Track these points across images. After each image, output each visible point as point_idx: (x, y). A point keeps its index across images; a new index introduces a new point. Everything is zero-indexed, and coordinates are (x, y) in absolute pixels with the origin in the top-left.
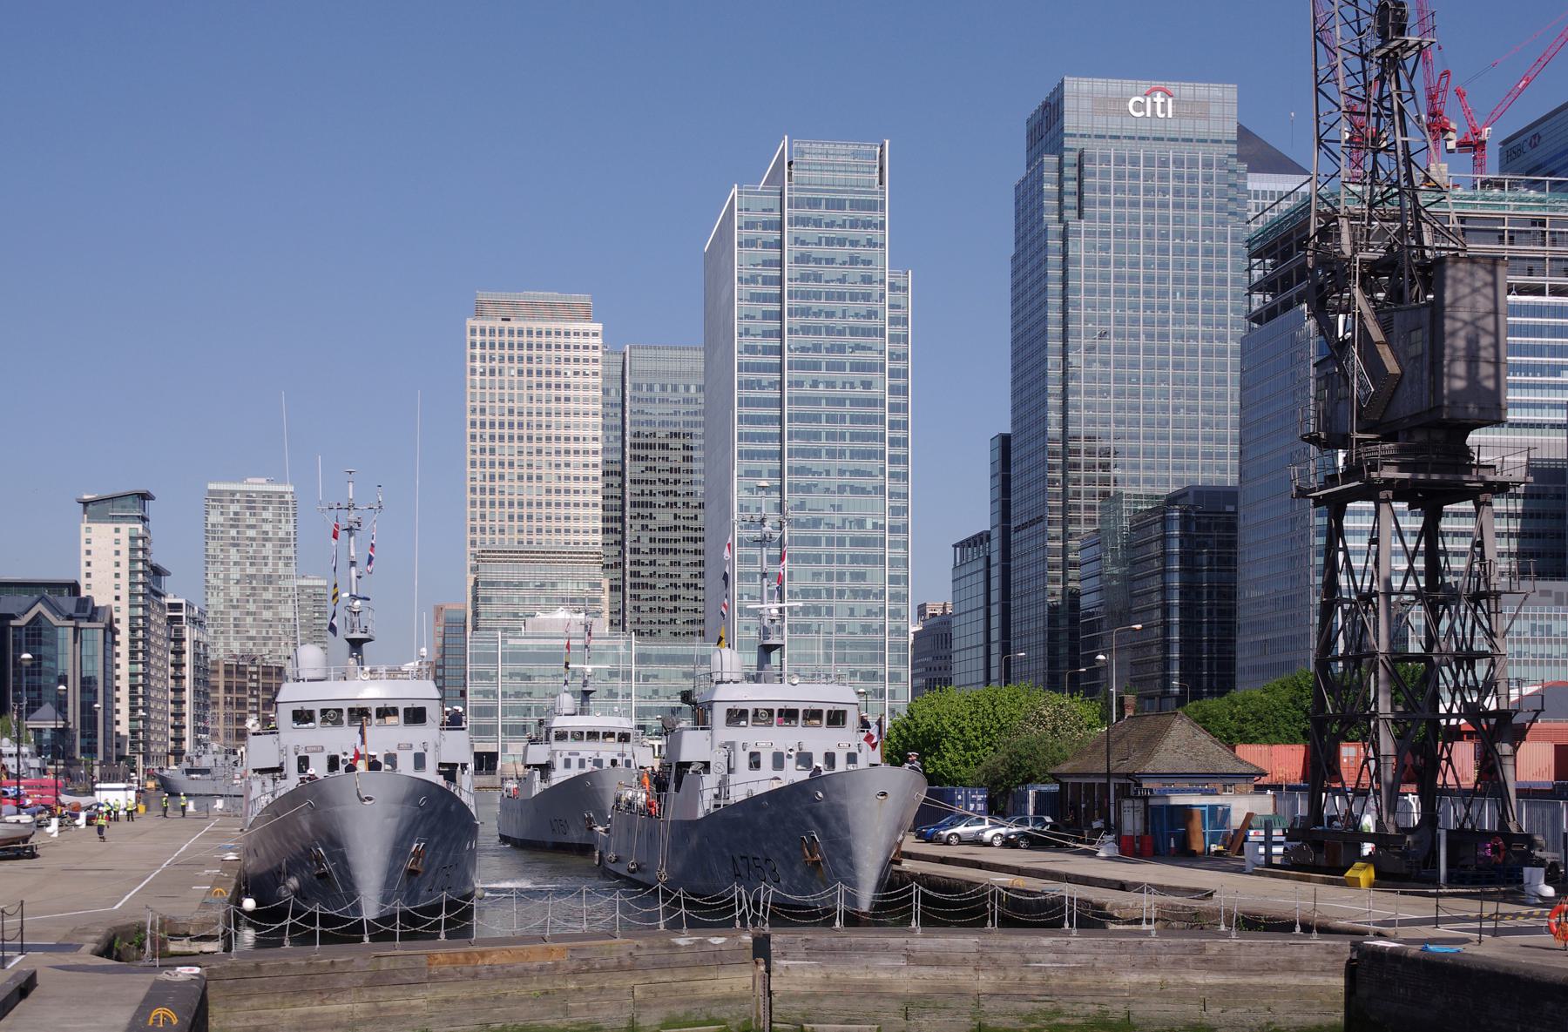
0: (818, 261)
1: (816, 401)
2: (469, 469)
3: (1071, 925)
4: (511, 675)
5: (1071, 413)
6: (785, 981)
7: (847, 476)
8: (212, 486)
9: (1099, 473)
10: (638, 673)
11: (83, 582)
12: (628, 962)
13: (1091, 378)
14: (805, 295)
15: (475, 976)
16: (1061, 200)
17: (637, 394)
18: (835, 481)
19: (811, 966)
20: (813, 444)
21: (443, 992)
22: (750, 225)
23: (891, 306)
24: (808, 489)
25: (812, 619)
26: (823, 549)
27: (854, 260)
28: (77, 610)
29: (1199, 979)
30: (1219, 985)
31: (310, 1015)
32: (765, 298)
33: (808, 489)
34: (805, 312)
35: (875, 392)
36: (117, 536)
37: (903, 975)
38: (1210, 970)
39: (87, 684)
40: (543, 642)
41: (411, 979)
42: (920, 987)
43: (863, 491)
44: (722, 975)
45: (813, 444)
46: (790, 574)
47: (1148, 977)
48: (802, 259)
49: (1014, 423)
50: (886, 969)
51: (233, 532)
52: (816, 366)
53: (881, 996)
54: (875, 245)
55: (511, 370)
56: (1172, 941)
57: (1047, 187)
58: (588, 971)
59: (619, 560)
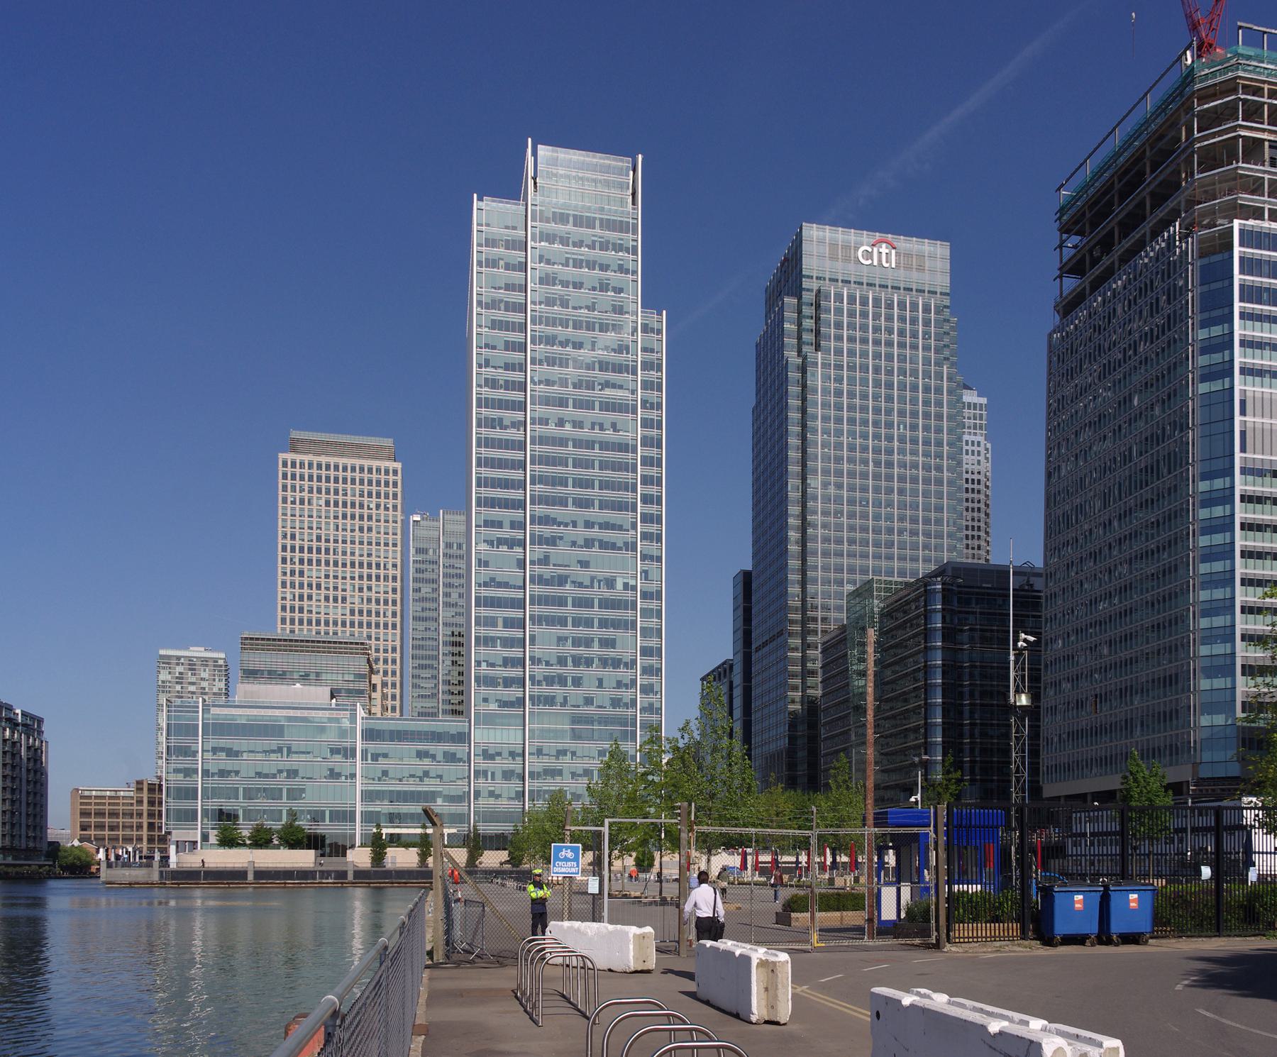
0: (565, 284)
1: (562, 442)
2: (280, 589)
4: (215, 750)
7: (568, 427)
8: (162, 652)
14: (551, 322)
16: (799, 338)
17: (448, 551)
18: (581, 533)
22: (491, 242)
23: (644, 350)
24: (552, 541)
25: (557, 690)
26: (569, 610)
27: (604, 287)
32: (506, 326)
33: (552, 541)
34: (550, 340)
35: (624, 436)
40: (255, 712)
43: (613, 546)
46: (533, 638)
48: (546, 280)
51: (178, 688)
54: (627, 272)
55: (319, 501)
57: (786, 325)
59: (435, 691)
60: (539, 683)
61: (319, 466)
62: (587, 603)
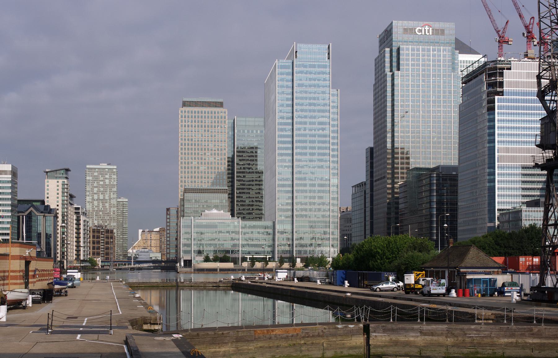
0: (306, 86)
1: (305, 135)
3: (394, 320)
4: (197, 233)
5: (396, 139)
6: (375, 341)
9: (405, 161)
10: (242, 232)
11: (46, 200)
12: (321, 334)
13: (403, 127)
15: (270, 338)
19: (385, 336)
20: (304, 151)
21: (260, 344)
28: (44, 210)
29: (530, 341)
30: (537, 343)
31: (215, 352)
35: (326, 132)
36: (58, 184)
37: (419, 339)
38: (534, 338)
39: (48, 236)
40: (208, 221)
41: (249, 339)
42: (426, 343)
44: (353, 338)
45: (304, 151)
47: (510, 340)
49: (374, 143)
50: (413, 337)
52: (305, 123)
53: (411, 346)
54: (326, 80)
56: (520, 327)
58: (308, 337)
60: (298, 211)
61: (195, 112)
62: (314, 185)
